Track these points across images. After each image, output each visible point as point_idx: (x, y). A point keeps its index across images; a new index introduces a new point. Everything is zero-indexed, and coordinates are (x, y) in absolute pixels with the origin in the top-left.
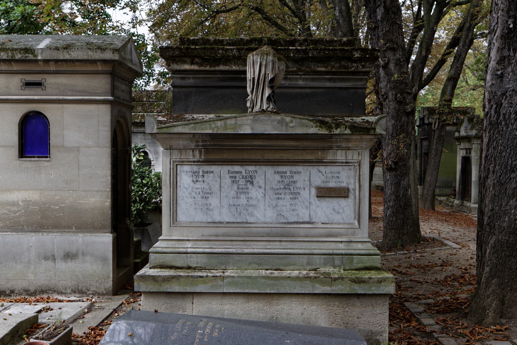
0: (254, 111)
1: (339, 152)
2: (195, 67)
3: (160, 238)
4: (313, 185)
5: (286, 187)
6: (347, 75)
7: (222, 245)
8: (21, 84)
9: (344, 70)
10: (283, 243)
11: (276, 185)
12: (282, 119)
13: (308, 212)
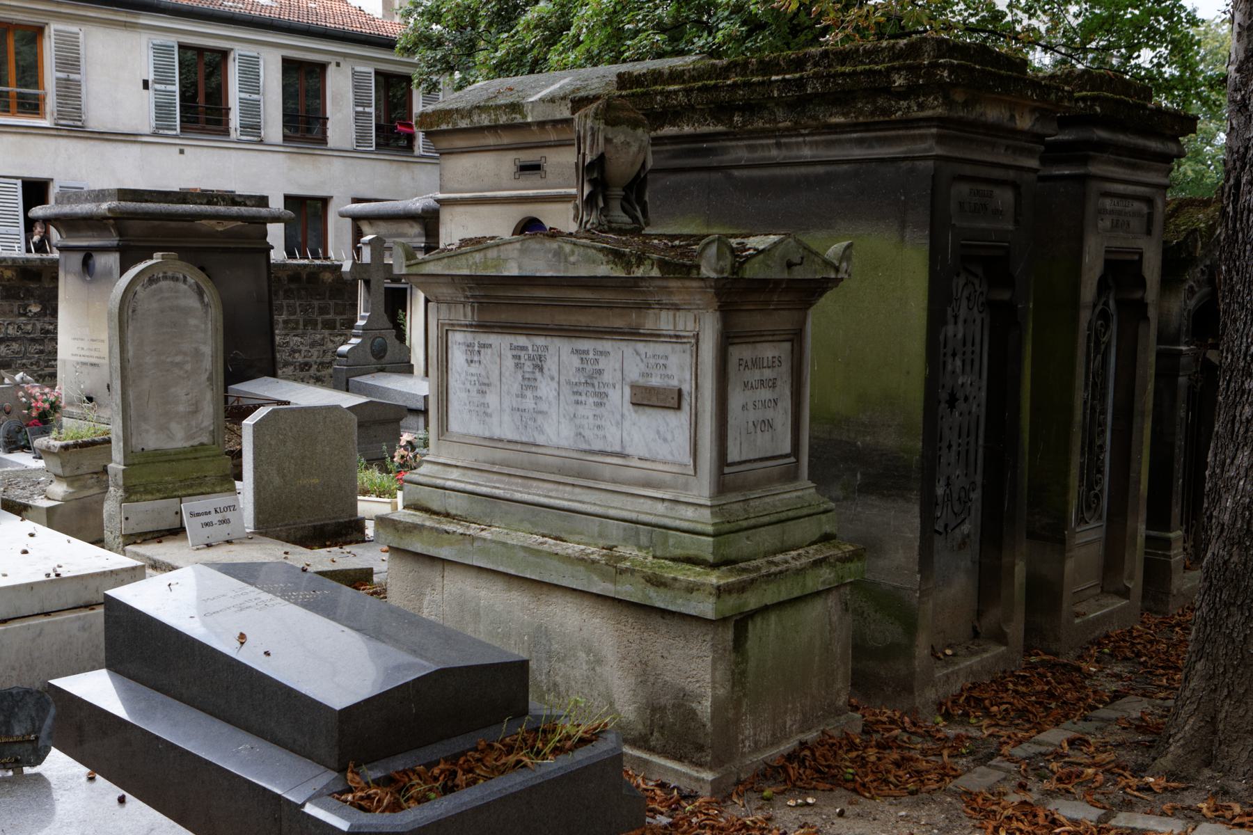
1: (664, 314)
4: (628, 380)
6: (894, 129)
8: (514, 169)
9: (882, 119)
10: (577, 490)
11: (574, 376)
12: (560, 247)
13: (619, 437)
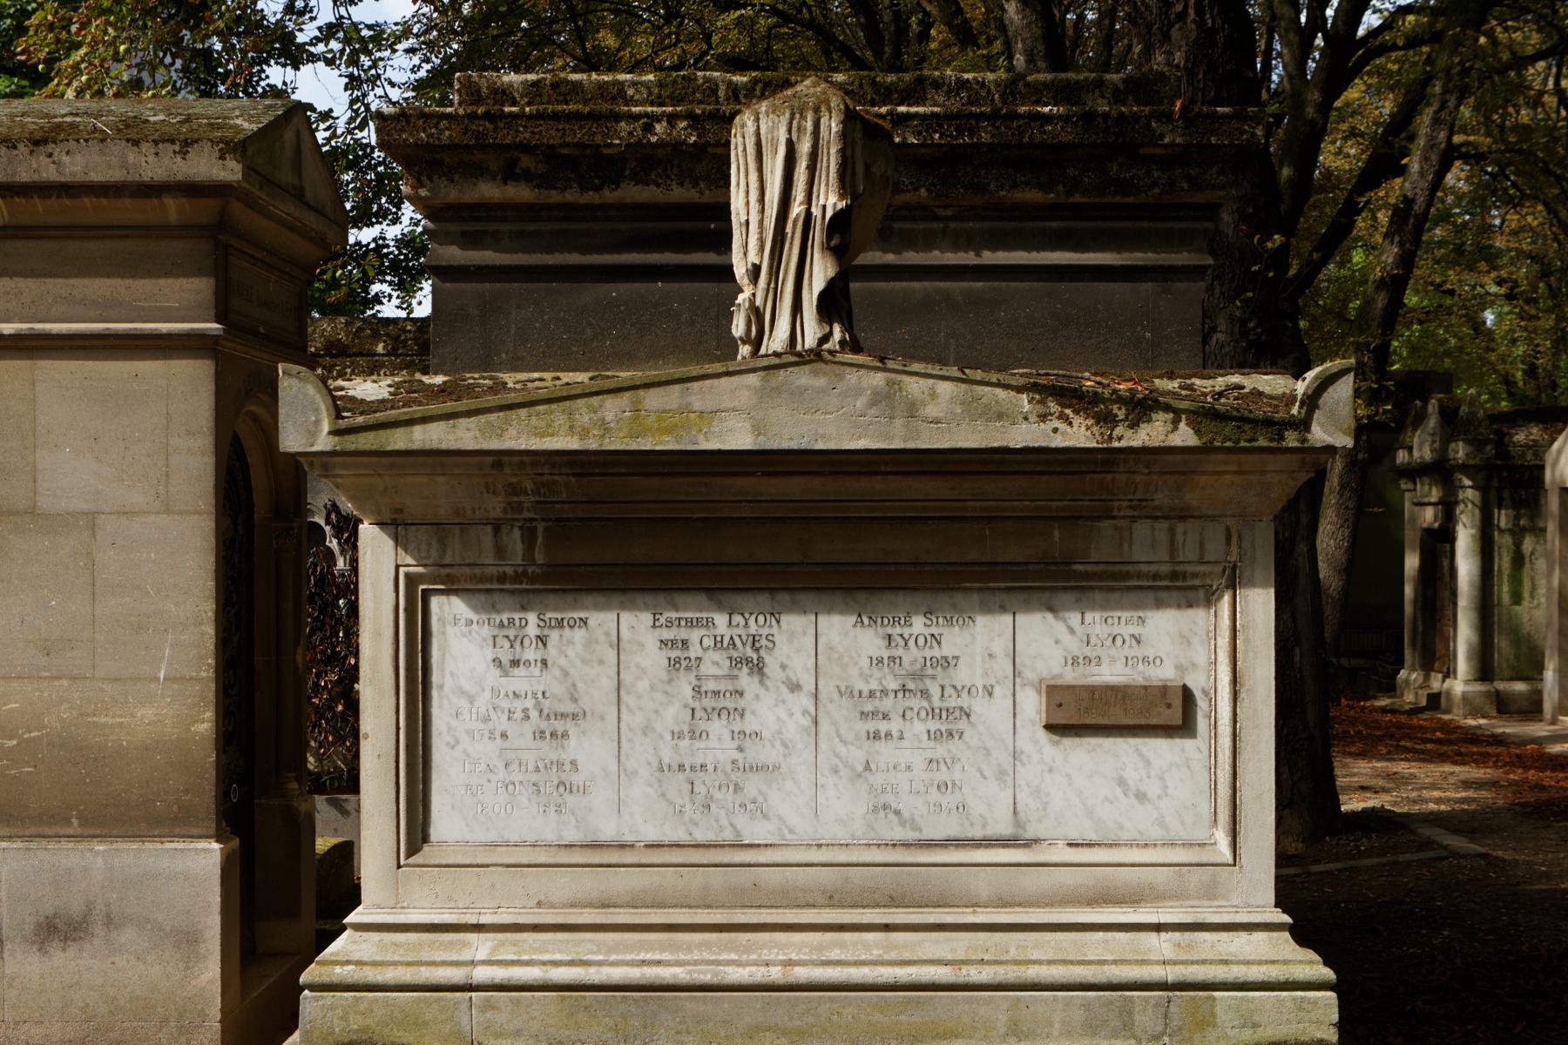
0: (763, 351)
1: (1142, 529)
2: (520, 193)
3: (351, 918)
4: (1029, 674)
5: (911, 685)
7: (629, 948)
9: (1118, 199)
11: (866, 678)
